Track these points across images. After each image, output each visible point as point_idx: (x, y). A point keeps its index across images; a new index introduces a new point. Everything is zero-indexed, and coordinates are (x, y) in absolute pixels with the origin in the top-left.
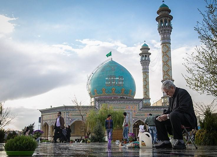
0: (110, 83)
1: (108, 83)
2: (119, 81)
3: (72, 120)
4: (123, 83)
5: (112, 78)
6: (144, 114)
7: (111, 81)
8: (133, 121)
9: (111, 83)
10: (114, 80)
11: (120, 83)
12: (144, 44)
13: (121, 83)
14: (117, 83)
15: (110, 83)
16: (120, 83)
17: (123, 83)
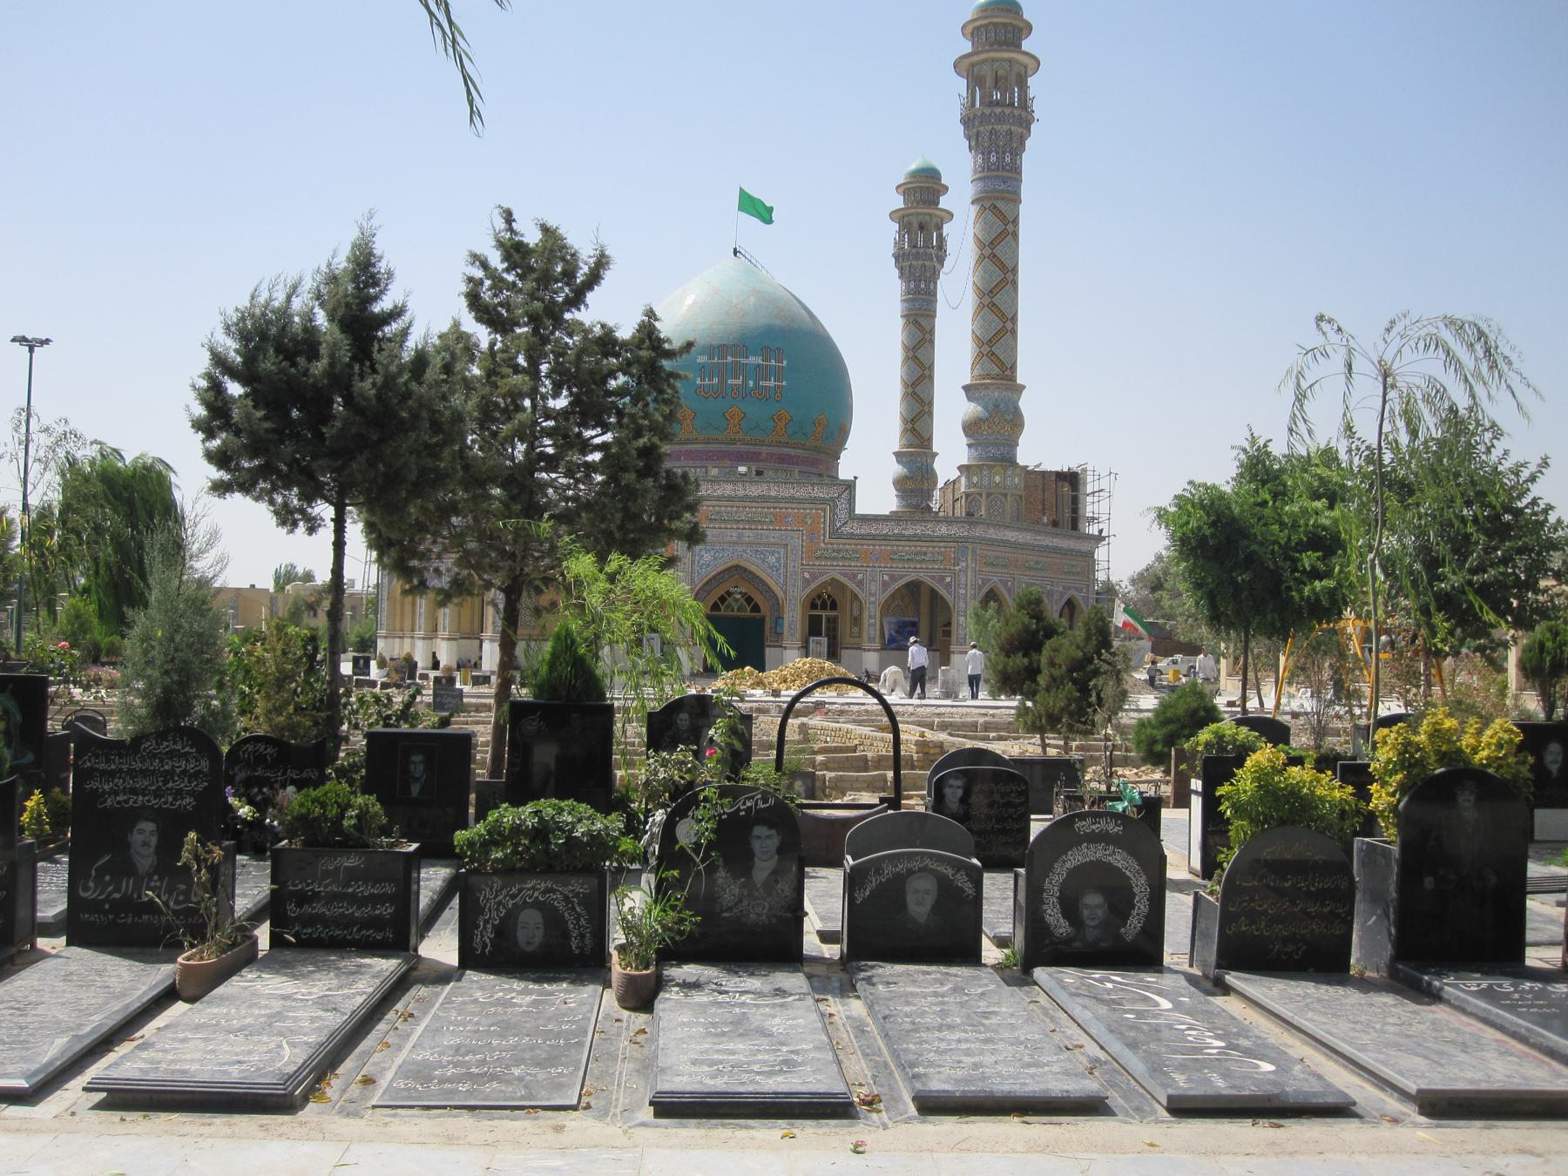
0: (716, 380)
1: (707, 382)
2: (762, 372)
3: (814, 577)
4: (784, 383)
5: (730, 359)
6: (855, 551)
7: (722, 371)
8: (943, 578)
9: (722, 382)
10: (737, 370)
11: (767, 383)
12: (1167, 960)
13: (772, 383)
14: (751, 383)
15: (716, 380)
16: (767, 383)
17: (784, 383)
